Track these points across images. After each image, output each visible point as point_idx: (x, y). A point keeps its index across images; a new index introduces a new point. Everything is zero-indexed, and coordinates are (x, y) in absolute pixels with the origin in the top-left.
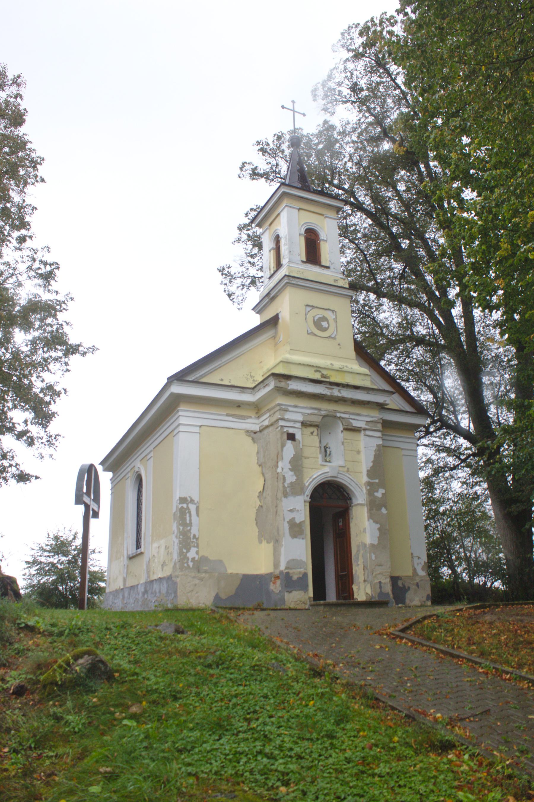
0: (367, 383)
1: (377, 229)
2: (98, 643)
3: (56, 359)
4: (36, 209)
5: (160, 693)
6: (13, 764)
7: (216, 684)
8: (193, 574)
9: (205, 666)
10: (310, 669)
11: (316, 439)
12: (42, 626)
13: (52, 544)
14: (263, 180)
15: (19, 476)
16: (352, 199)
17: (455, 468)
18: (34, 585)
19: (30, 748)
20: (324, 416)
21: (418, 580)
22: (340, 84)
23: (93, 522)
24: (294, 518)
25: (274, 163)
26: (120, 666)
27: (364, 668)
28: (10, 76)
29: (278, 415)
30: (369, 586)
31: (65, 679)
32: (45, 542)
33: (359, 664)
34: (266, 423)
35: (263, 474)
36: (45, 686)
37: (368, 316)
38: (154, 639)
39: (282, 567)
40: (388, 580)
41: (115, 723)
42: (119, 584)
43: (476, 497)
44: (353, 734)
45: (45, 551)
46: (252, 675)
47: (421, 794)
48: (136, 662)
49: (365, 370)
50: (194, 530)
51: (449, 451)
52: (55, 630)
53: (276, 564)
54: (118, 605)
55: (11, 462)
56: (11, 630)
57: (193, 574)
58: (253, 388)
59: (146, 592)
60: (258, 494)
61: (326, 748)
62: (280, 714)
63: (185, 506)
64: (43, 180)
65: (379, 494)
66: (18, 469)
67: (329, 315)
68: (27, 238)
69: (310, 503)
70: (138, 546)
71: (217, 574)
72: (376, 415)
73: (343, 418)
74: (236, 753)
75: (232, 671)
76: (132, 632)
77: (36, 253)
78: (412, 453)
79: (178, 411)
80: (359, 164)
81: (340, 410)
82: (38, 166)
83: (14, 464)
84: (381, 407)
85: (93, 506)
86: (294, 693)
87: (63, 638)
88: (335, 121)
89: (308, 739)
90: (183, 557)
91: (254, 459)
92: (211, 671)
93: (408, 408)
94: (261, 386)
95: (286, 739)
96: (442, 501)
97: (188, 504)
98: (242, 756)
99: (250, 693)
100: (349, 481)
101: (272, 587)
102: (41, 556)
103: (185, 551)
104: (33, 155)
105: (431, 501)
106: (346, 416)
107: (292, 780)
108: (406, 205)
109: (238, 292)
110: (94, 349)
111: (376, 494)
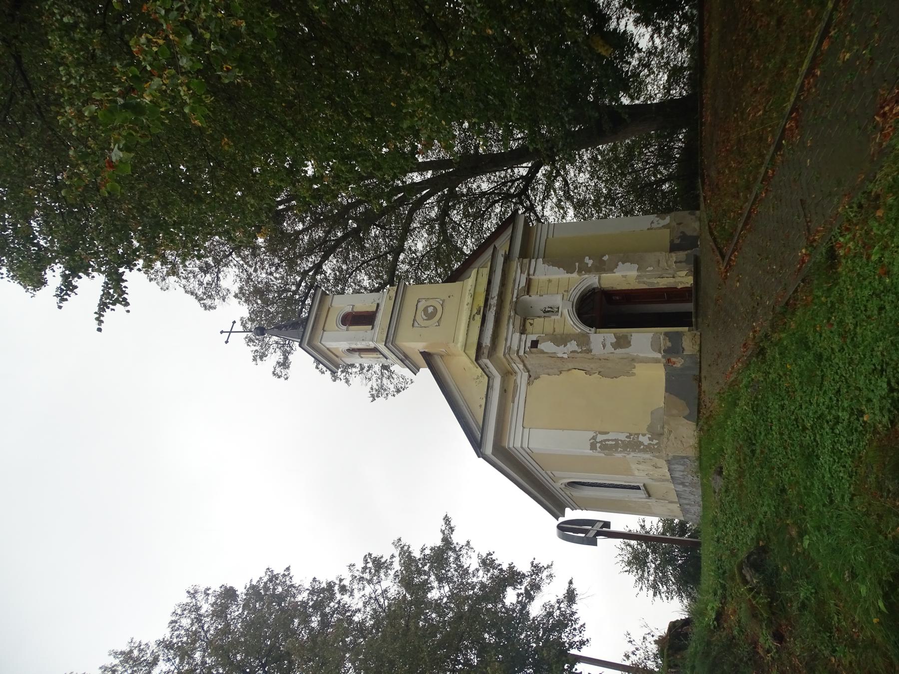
0: (485, 271)
1: (338, 250)
2: (732, 552)
3: (457, 558)
4: (315, 578)
5: (779, 505)
6: (845, 656)
7: (771, 451)
8: (665, 440)
9: (754, 456)
10: (757, 357)
11: (537, 320)
12: (717, 604)
13: (636, 568)
14: (290, 357)
15: (569, 602)
16: (311, 274)
17: (565, 180)
18: (678, 589)
19: (830, 637)
20: (516, 313)
21: (674, 224)
22: (201, 284)
23: (614, 528)
24: (612, 344)
25: (275, 345)
26: (752, 539)
27: (758, 304)
28: (189, 600)
29: (515, 356)
30: (679, 273)
31: (765, 594)
32: (632, 578)
33: (754, 307)
34: (521, 366)
35: (569, 370)
36: (773, 614)
37: (421, 261)
38: (727, 498)
39: (659, 356)
40: (673, 254)
41: (806, 553)
42: (676, 507)
43: (594, 159)
44: (818, 337)
45: (642, 576)
46: (762, 414)
47: (873, 293)
48: (750, 520)
49: (474, 273)
50: (622, 437)
51: (549, 187)
52: (719, 592)
53: (656, 361)
54: (696, 509)
55: (556, 608)
56: (720, 636)
57: (665, 440)
58: (489, 377)
59: (683, 484)
60: (588, 376)
61: (830, 365)
62: (799, 399)
63: (598, 445)
64: (288, 569)
65: (590, 262)
66: (562, 602)
67: (422, 305)
68: (342, 584)
69: (597, 328)
70: (638, 488)
71: (665, 417)
72: (515, 264)
73: (518, 295)
74: (832, 452)
75: (758, 431)
76: (721, 518)
77: (356, 577)
78: (551, 228)
79: (509, 448)
80: (278, 266)
81: (511, 296)
82: (275, 573)
83: (558, 605)
84: (507, 258)
85: (597, 527)
86: (780, 380)
87: (727, 585)
88: (235, 289)
89: (822, 379)
90: (648, 449)
91: (554, 378)
92: (758, 451)
93: (509, 231)
94: (486, 370)
95: (822, 400)
96: (597, 191)
97: (597, 442)
98: (836, 447)
99: (779, 420)
100: (576, 290)
101: (678, 365)
102: (648, 581)
103: (642, 447)
104: (265, 579)
105: (597, 204)
106: (516, 292)
107: (858, 407)
108: (316, 223)
109: (395, 381)
110: (447, 520)
111: (590, 265)
